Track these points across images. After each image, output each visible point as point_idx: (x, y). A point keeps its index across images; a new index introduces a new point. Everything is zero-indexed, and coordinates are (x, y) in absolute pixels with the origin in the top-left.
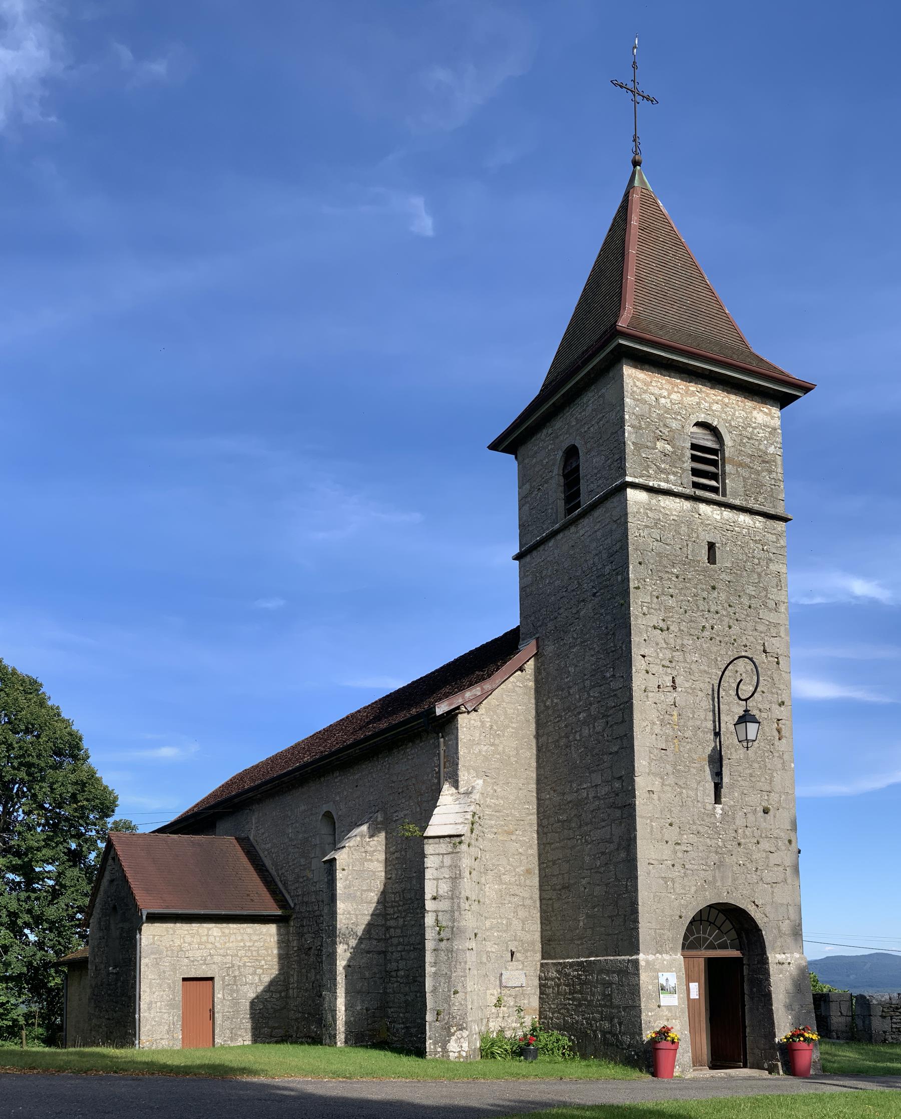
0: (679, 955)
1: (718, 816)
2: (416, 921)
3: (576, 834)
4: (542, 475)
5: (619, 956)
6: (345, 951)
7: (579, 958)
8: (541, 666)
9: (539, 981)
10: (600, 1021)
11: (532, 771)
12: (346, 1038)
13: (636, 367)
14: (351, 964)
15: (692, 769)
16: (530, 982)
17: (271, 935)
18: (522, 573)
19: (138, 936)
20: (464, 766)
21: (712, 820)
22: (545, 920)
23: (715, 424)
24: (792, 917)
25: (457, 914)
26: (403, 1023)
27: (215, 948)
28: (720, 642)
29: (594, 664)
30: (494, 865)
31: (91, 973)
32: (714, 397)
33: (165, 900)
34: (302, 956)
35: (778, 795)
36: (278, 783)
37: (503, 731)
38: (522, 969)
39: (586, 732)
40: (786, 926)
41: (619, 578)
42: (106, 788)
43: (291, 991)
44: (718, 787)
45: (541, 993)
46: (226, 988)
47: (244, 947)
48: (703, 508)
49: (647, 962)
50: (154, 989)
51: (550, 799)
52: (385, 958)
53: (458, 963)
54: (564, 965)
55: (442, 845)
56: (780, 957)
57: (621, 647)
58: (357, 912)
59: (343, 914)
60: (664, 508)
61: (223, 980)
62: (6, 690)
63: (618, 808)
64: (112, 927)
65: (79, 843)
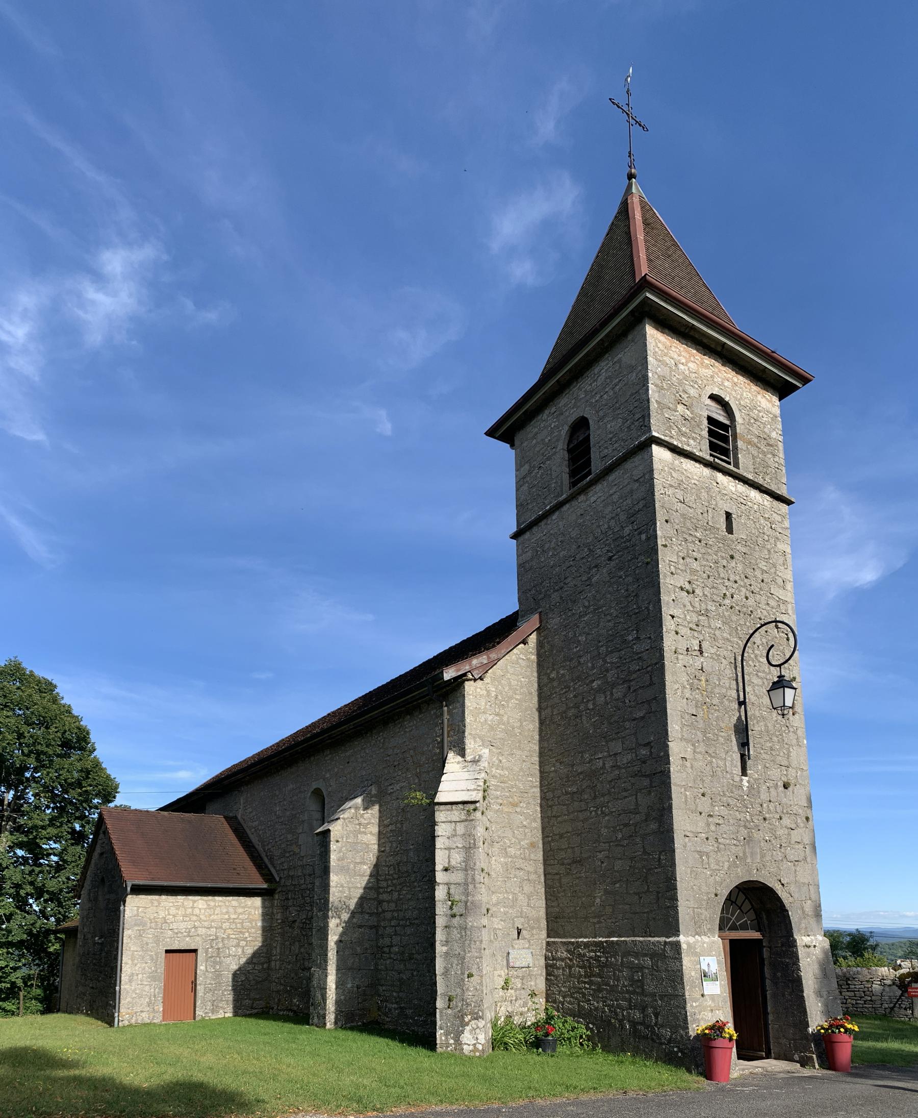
0: (717, 937)
1: (745, 789)
2: (413, 894)
3: (590, 805)
4: (543, 454)
5: (651, 936)
6: (337, 926)
7: (595, 938)
8: (544, 640)
9: (546, 960)
10: (627, 1009)
11: (535, 744)
12: (336, 1018)
13: (657, 329)
14: (343, 939)
15: (720, 738)
16: (536, 962)
17: (255, 908)
18: (520, 551)
19: (122, 908)
20: (470, 734)
21: (740, 793)
22: (551, 895)
23: (727, 399)
24: (813, 897)
25: (471, 887)
26: (397, 1003)
27: (200, 920)
28: (739, 611)
29: (611, 630)
30: (499, 837)
31: (80, 942)
32: (725, 375)
33: (151, 872)
34: (286, 929)
35: (795, 771)
36: (267, 764)
37: (507, 702)
38: (528, 948)
39: (601, 699)
40: (808, 907)
41: (643, 537)
42: (108, 777)
43: (273, 964)
44: (744, 759)
45: (548, 974)
46: (209, 959)
47: (228, 919)
48: (720, 476)
49: (688, 944)
50: (136, 961)
51: (555, 771)
52: (377, 933)
53: (473, 943)
54: (578, 945)
55: (455, 812)
56: (806, 940)
57: (647, 608)
58: (350, 885)
59: (336, 887)
60: (686, 470)
61: (207, 952)
62: (22, 688)
63: (645, 776)
64: (100, 898)
65: (82, 824)
